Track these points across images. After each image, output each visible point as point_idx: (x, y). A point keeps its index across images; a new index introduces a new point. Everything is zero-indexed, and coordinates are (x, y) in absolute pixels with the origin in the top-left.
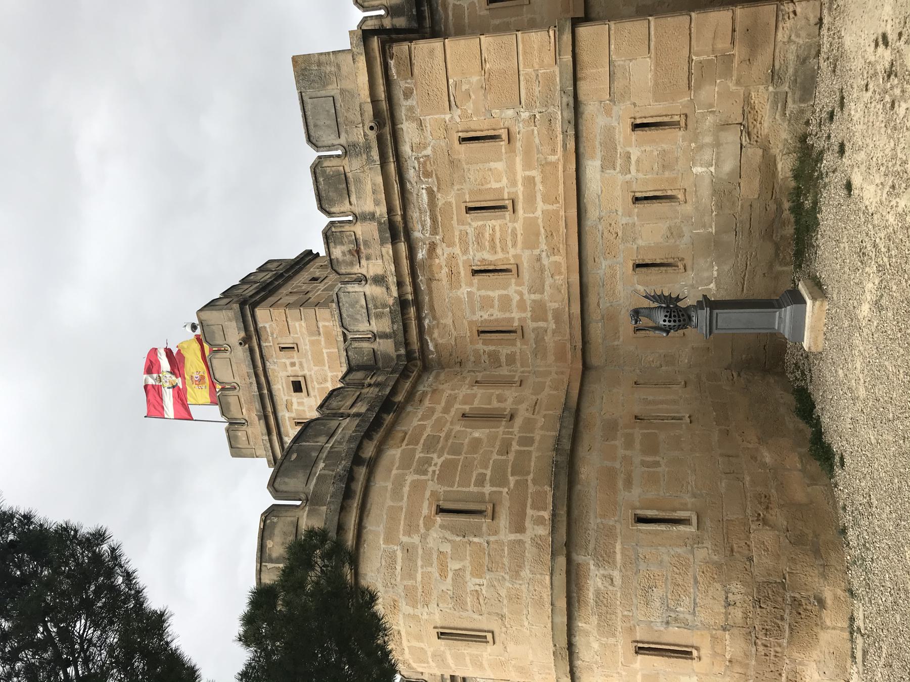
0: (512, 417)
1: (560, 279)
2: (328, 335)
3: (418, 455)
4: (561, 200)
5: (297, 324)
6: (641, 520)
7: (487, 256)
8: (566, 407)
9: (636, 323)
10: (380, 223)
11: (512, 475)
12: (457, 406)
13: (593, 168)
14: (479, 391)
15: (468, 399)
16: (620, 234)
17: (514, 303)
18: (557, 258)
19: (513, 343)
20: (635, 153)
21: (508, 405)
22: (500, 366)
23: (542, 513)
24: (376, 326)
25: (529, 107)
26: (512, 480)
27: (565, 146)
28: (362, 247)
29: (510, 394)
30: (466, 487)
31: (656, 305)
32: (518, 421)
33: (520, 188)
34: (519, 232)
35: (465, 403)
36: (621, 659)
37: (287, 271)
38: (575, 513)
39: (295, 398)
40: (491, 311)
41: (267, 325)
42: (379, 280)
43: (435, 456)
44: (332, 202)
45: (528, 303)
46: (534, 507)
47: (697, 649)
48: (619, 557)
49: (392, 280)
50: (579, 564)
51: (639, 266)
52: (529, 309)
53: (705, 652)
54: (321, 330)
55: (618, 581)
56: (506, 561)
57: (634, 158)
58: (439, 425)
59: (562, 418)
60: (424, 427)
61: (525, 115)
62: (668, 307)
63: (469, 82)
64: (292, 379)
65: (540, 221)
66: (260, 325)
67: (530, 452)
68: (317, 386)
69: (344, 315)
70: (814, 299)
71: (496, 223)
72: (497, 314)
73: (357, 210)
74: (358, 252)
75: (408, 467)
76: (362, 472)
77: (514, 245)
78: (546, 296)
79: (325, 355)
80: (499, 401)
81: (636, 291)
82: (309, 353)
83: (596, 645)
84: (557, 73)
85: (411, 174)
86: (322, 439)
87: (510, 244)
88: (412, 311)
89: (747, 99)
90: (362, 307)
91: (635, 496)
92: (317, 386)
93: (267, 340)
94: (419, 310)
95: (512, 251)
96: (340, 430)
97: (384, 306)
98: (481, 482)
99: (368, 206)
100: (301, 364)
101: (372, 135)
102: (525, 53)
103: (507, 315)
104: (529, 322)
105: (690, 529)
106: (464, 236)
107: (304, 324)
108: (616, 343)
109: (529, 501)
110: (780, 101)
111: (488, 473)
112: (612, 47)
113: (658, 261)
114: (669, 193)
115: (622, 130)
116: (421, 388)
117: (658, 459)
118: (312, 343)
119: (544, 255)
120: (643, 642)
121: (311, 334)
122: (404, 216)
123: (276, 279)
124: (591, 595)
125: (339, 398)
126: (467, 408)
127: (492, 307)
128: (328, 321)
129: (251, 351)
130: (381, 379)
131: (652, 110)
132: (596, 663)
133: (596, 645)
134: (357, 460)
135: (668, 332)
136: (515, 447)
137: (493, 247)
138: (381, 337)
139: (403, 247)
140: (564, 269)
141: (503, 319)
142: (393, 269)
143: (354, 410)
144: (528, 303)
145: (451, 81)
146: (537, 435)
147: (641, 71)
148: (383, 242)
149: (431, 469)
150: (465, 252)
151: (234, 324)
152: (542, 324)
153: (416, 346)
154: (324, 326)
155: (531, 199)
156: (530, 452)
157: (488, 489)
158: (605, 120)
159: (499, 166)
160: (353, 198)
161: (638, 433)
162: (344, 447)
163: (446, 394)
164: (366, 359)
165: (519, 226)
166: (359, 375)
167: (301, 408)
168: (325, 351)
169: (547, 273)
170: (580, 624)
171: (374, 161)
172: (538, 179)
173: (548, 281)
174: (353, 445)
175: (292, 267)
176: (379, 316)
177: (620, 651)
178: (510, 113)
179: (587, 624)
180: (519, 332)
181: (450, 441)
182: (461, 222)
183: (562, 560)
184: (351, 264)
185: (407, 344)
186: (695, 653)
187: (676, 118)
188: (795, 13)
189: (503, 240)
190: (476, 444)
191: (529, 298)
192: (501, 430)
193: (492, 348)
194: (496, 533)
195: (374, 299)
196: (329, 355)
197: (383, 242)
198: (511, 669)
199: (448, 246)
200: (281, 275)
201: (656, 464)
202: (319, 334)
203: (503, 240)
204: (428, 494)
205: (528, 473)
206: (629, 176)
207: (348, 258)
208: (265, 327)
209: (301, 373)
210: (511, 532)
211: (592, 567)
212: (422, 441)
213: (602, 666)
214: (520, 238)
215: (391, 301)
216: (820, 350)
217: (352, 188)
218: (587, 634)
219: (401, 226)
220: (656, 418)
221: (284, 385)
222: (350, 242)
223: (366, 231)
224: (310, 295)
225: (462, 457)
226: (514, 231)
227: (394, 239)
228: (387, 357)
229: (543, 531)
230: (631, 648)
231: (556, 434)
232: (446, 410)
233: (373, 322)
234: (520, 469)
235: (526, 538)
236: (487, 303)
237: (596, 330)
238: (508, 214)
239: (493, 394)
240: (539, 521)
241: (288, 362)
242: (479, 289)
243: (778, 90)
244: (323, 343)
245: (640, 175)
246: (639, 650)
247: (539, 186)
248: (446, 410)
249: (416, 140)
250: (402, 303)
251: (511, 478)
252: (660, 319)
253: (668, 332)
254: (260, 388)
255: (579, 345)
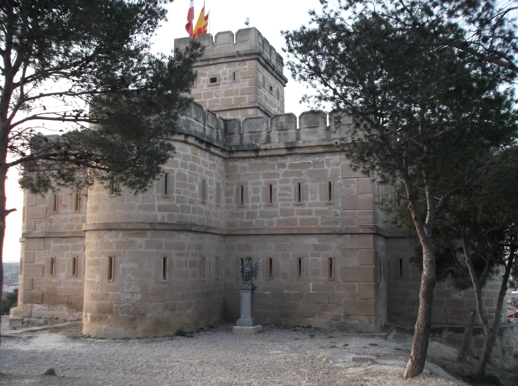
0: (204, 203)
1: (266, 225)
2: (241, 100)
3: (188, 163)
4: (301, 227)
5: (247, 83)
6: (165, 259)
7: (278, 192)
8: (208, 228)
9: (246, 259)
10: (295, 142)
11: (181, 206)
12: (208, 177)
13: (314, 240)
14: (214, 187)
15: (211, 182)
16: (285, 252)
17: (255, 204)
18: (275, 224)
19: (237, 202)
20: (320, 259)
21: (208, 201)
22: (226, 196)
23: (166, 218)
24: (246, 135)
25: (342, 214)
26: (179, 205)
27: (324, 229)
28: (284, 132)
29: (213, 202)
30: (176, 185)
31: (253, 267)
32: (202, 206)
33: (307, 208)
34: (289, 207)
35: (209, 181)
36: (106, 251)
37: (276, 72)
38: (167, 232)
39: (207, 78)
40: (252, 192)
41: (247, 66)
42: (268, 140)
43: (188, 170)
44: (306, 119)
45: (256, 210)
46: (169, 215)
47: (113, 281)
48: (149, 250)
49: (268, 146)
50: (146, 234)
51: (271, 260)
52: (253, 210)
53: (112, 284)
54: (244, 96)
55: (140, 250)
56: (146, 203)
57: (317, 258)
58: (201, 170)
59: (203, 226)
60: (199, 163)
61: (339, 212)
62: (252, 272)
63: (354, 188)
64: (218, 78)
65: (292, 217)
66: (247, 62)
67: (190, 213)
68: (214, 91)
69: (252, 120)
70: (254, 329)
71: (293, 197)
72: (251, 195)
73: (301, 131)
74: (282, 129)
75: (184, 159)
76: (182, 138)
77: (283, 205)
78: (259, 219)
79: (230, 97)
80: (210, 197)
81: (259, 258)
82: (231, 89)
83: (111, 240)
84: (355, 226)
85: (317, 158)
86: (194, 116)
87: (283, 202)
88: (253, 154)
89: (338, 305)
90: (256, 129)
91: (174, 257)
92: (214, 91)
93: (239, 65)
94: (253, 157)
95: (280, 204)
96: (198, 123)
97: (256, 141)
98: (179, 192)
99: (303, 137)
100: (226, 83)
101: (334, 142)
102: (365, 212)
103: (250, 200)
104: (246, 210)
105: (162, 280)
106: (287, 181)
107: (248, 86)
108: (236, 250)
109: (171, 213)
110: (337, 318)
111: (182, 195)
112: (364, 250)
113: (272, 268)
114: (302, 273)
115: (329, 253)
116: (216, 158)
117: (188, 266)
118: (237, 90)
119: (277, 218)
120: (114, 259)
121: (242, 90)
122: (297, 154)
123: (272, 67)
124: (133, 239)
125: (212, 119)
126: (207, 182)
127: (254, 193)
128: (248, 101)
129: (234, 57)
130: (221, 137)
131: (338, 267)
132: (103, 240)
133: (111, 240)
134: (187, 136)
135: (241, 272)
136: (192, 206)
137: (281, 195)
138: (241, 138)
139: (284, 152)
140: (270, 227)
141: (248, 199)
142: (273, 147)
143: (207, 127)
144: (256, 210)
145: (355, 179)
146: (197, 216)
147: (354, 262)
148: (286, 143)
149: (183, 169)
150: (280, 182)
151: (248, 48)
152: (245, 216)
153: (236, 155)
154: (246, 98)
155: (302, 213)
156: (190, 213)
157: (175, 195)
158: (334, 245)
159: (318, 200)
160: (307, 130)
161: (198, 259)
162: (192, 128)
163: (212, 171)
164: (230, 129)
165: (291, 207)
166: (222, 126)
167: (202, 81)
168: (233, 97)
169: (269, 220)
170: (121, 234)
171: (323, 142)
172: (311, 217)
173: (265, 220)
174: (193, 134)
175: (279, 74)
176: (251, 137)
177: (110, 250)
178: (340, 205)
179: (120, 236)
180: (242, 206)
181: (194, 176)
182: (294, 181)
183: (148, 227)
184: (276, 126)
185: (237, 151)
186: (111, 280)
187: (333, 276)
188: (371, 323)
189: (285, 200)
190: (193, 188)
191: (258, 211)
192: (199, 199)
193: (234, 192)
194: (158, 199)
195: (260, 136)
196: (231, 99)
197: (286, 143)
198: (97, 203)
199: (283, 174)
200: (274, 70)
201: (186, 266)
202: (242, 95)
203: (285, 200)
204: (173, 168)
205: (182, 212)
206: (310, 256)
207: (279, 125)
208: (246, 65)
209: (221, 83)
210: (158, 205)
211: (145, 239)
212: (194, 163)
213: (101, 243)
214: (286, 207)
215: (258, 145)
216: (234, 332)
217: (311, 130)
218: (117, 236)
219: (293, 152)
220: (204, 266)
221: (214, 73)
222: (287, 127)
223: (291, 137)
224: (263, 88)
225: (188, 183)
226: (289, 205)
227: (288, 149)
228: (230, 140)
229: (159, 219)
230: (111, 255)
231: (197, 223)
232: (207, 173)
233: (248, 134)
234: (184, 209)
235: (156, 212)
236: (256, 191)
237: (242, 241)
238: (297, 202)
239: (213, 193)
240: (163, 217)
241: (227, 76)
242: (263, 187)
243: (342, 317)
244: (237, 96)
245: (310, 261)
246: (111, 259)
247: (307, 217)
248: (207, 173)
249: (331, 162)
250: (257, 150)
251: (180, 205)
252: (248, 269)
253: (241, 272)
254: (213, 59)
255: (235, 233)
